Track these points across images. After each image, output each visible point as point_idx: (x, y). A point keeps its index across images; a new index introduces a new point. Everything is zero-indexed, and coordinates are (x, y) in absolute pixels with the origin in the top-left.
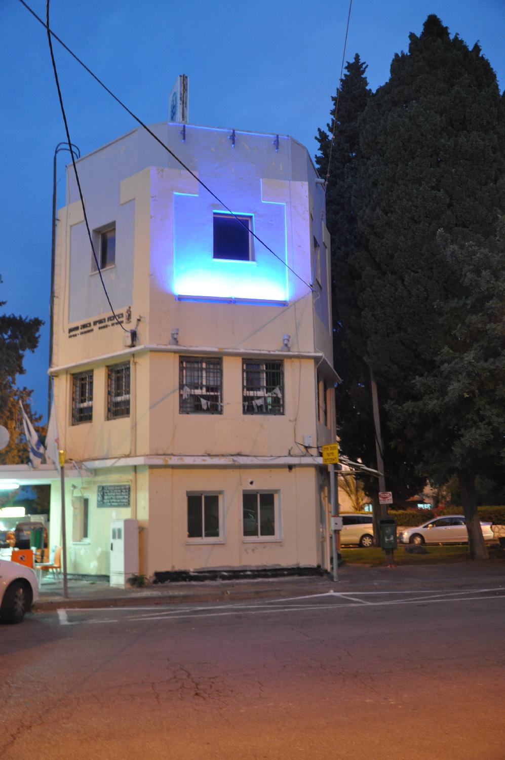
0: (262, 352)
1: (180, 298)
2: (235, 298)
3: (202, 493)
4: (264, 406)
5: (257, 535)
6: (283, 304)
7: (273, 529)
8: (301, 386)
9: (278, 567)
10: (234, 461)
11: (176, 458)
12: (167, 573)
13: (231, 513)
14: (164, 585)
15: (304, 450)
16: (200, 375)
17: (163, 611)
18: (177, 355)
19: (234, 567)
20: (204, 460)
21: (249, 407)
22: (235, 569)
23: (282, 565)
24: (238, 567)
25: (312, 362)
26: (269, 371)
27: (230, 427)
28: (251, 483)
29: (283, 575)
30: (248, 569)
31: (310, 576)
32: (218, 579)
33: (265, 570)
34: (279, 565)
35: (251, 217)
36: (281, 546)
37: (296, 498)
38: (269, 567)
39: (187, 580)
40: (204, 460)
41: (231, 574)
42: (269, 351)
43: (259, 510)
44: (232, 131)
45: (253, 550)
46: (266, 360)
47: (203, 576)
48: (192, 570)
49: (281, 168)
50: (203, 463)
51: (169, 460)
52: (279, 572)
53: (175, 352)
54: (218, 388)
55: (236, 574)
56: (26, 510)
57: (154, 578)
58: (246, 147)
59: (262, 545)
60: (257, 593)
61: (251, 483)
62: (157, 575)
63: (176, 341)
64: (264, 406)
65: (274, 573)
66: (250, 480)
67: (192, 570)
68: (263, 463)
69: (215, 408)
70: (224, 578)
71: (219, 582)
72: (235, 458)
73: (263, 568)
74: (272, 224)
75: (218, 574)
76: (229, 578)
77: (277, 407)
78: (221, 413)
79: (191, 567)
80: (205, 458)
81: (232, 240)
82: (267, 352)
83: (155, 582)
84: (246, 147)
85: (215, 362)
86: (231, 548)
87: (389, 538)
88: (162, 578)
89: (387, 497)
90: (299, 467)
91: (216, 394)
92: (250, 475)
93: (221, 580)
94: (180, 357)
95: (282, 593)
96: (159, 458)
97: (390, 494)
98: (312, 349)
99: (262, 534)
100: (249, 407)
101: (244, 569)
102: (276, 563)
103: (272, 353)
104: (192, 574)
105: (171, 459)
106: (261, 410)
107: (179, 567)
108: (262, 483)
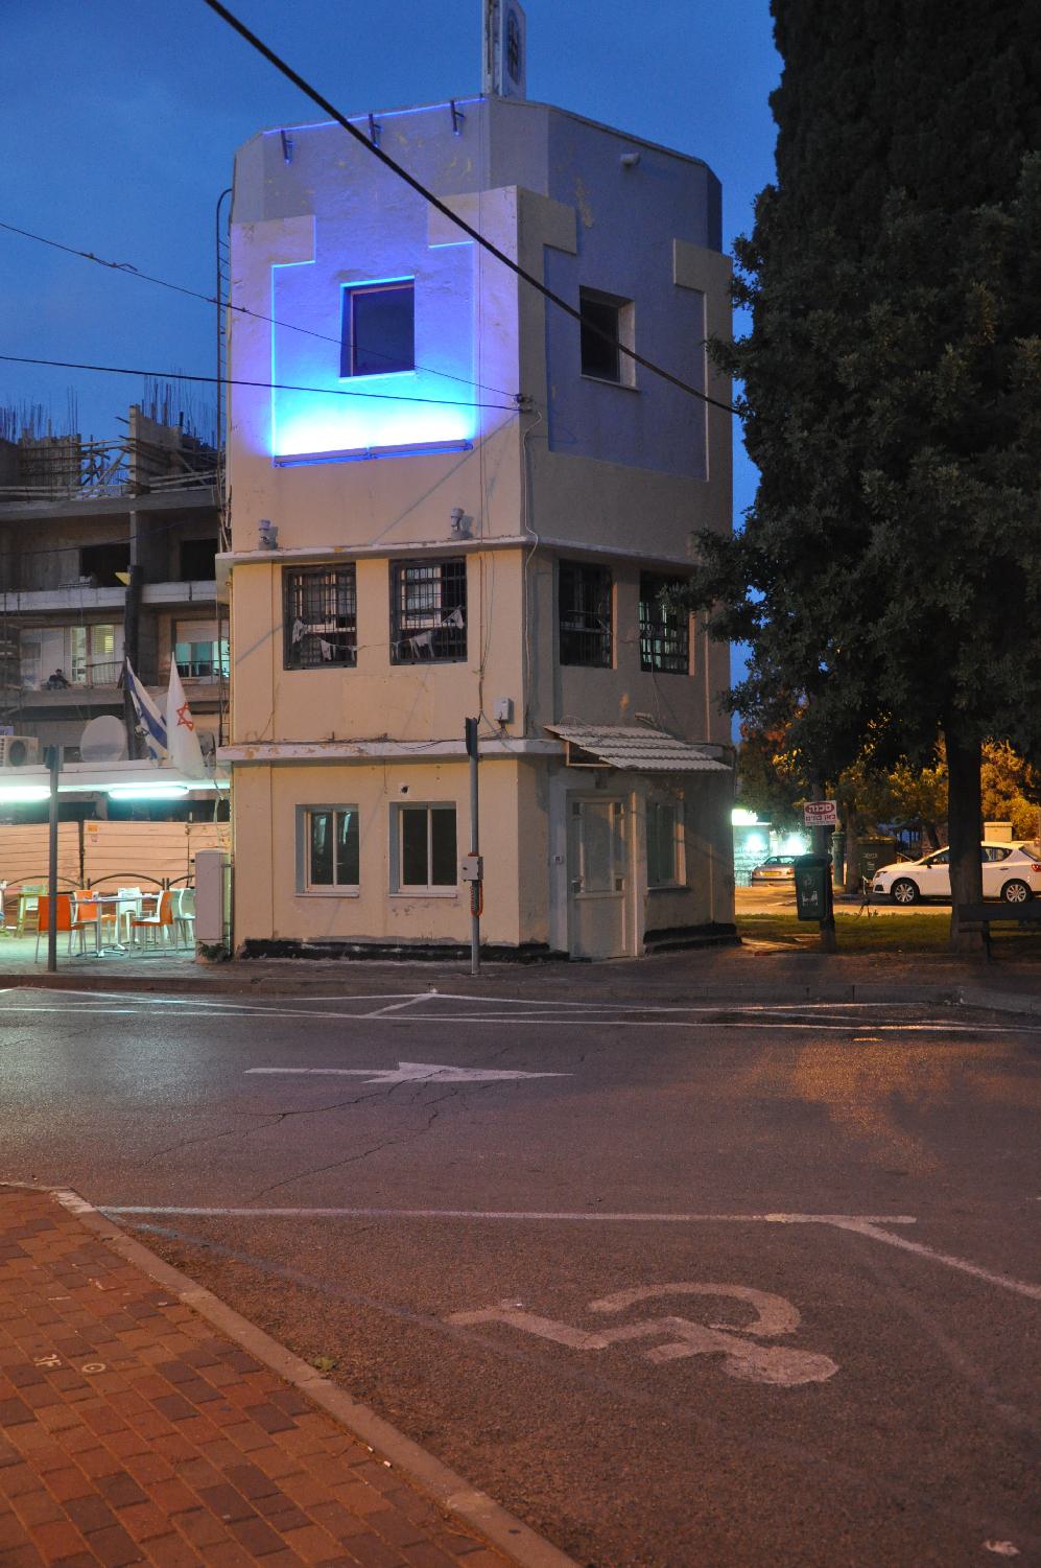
0: (412, 546)
1: (282, 462)
2: (371, 448)
3: (427, 804)
4: (431, 648)
5: (425, 883)
6: (465, 446)
7: (456, 879)
8: (500, 604)
9: (451, 943)
10: (361, 751)
11: (266, 748)
12: (265, 942)
13: (378, 849)
14: (257, 961)
15: (498, 727)
16: (430, 592)
17: (522, 1007)
18: (278, 567)
19: (375, 939)
20: (311, 751)
21: (404, 651)
22: (377, 943)
23: (456, 938)
24: (381, 939)
25: (518, 553)
26: (445, 578)
27: (375, 693)
28: (405, 790)
29: (455, 958)
30: (398, 943)
31: (503, 961)
32: (343, 958)
33: (427, 947)
34: (452, 939)
35: (411, 282)
36: (456, 905)
37: (496, 819)
38: (435, 940)
39: (294, 955)
40: (311, 751)
41: (366, 950)
42: (424, 543)
43: (429, 844)
44: (449, 105)
45: (406, 911)
46: (441, 558)
47: (319, 951)
48: (305, 940)
49: (469, 168)
50: (309, 756)
51: (255, 753)
52: (451, 952)
53: (274, 561)
54: (348, 620)
55: (374, 950)
56: (735, 807)
57: (244, 949)
58: (402, 140)
59: (423, 901)
60: (305, 984)
61: (405, 790)
62: (249, 943)
63: (270, 543)
64: (431, 648)
65: (439, 952)
66: (401, 785)
67: (305, 940)
68: (410, 753)
69: (343, 653)
70: (353, 956)
71: (345, 961)
72: (363, 746)
73: (424, 943)
74: (447, 288)
75: (346, 948)
76: (362, 956)
77: (450, 646)
78: (395, 661)
79: (305, 935)
80: (312, 747)
81: (379, 337)
82: (420, 546)
83: (244, 956)
84: (402, 140)
85: (342, 570)
86: (378, 907)
87: (809, 897)
88: (255, 948)
89: (825, 812)
90: (391, 764)
91: (349, 629)
92: (400, 776)
93: (347, 958)
94: (391, 562)
95: (349, 989)
96: (239, 750)
97: (833, 806)
98: (516, 528)
99: (434, 883)
100: (404, 651)
101: (393, 943)
102: (446, 934)
103: (429, 546)
104: (304, 946)
105: (258, 750)
106: (424, 656)
107: (285, 934)
108: (428, 788)
